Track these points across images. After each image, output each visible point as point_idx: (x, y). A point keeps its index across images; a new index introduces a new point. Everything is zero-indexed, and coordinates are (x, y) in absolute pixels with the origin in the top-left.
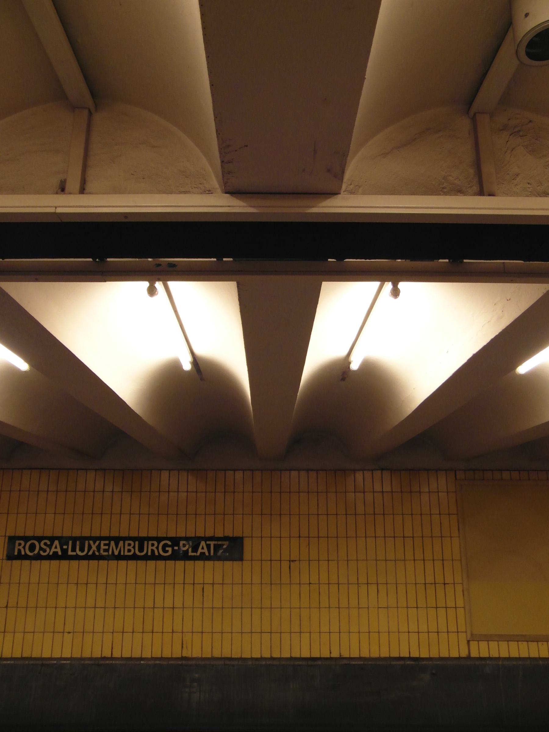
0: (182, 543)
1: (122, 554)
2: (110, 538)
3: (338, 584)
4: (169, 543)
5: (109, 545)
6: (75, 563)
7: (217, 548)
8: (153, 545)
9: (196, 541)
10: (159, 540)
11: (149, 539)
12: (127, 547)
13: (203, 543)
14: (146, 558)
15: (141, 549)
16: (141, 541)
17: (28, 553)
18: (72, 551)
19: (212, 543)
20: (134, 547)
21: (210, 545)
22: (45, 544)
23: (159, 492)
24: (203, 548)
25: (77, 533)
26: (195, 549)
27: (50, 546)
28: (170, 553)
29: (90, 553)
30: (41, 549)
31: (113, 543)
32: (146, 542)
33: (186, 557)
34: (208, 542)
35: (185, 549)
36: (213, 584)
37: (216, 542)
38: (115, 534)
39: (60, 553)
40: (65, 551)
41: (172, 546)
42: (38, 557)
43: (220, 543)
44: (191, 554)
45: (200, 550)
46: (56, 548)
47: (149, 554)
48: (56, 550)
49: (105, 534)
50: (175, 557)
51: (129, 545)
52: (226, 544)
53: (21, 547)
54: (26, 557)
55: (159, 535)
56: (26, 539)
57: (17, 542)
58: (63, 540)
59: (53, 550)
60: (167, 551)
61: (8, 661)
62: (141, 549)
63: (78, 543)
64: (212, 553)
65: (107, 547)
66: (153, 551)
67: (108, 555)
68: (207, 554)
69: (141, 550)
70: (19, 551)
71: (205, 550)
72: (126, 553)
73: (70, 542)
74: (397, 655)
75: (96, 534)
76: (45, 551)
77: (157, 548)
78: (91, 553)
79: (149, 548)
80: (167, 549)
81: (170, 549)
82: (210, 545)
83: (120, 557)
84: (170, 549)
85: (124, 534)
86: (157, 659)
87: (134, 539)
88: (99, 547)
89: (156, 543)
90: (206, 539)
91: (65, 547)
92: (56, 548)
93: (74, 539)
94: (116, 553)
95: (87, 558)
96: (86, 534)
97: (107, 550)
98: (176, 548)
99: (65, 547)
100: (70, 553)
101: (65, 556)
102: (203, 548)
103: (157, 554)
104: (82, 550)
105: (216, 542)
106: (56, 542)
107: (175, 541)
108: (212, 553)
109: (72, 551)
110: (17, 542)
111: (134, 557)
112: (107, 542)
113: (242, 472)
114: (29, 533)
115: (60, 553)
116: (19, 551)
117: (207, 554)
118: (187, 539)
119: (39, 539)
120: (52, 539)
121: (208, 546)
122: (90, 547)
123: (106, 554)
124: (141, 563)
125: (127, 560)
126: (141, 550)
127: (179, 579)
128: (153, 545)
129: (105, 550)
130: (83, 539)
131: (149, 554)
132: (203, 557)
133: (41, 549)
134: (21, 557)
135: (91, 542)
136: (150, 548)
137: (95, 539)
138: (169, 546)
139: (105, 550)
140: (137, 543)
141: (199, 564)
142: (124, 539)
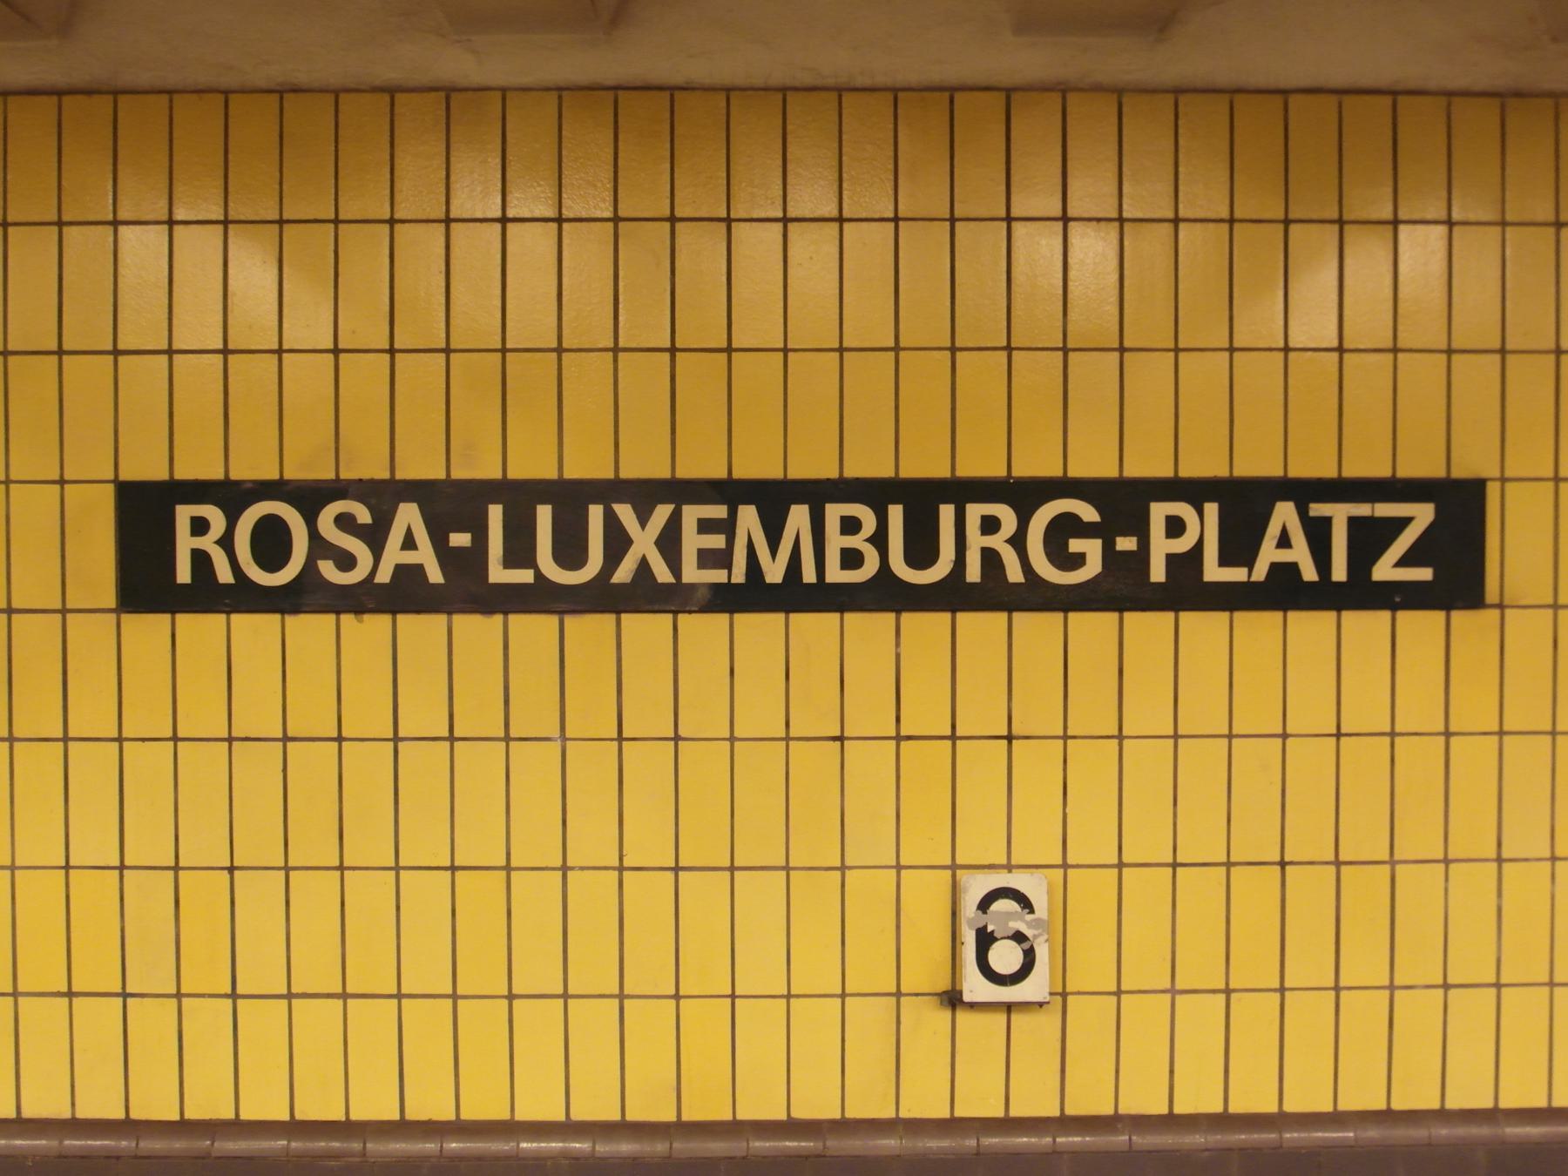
0: (1159, 512)
1: (809, 576)
2: (731, 491)
3: (732, 739)
4: (1088, 513)
5: (728, 527)
6: (534, 629)
7: (1370, 539)
8: (990, 525)
9: (1244, 505)
10: (1025, 494)
11: (963, 491)
12: (836, 541)
13: (1285, 514)
14: (953, 596)
15: (921, 550)
16: (921, 499)
18: (510, 562)
19: (1340, 514)
20: (880, 540)
21: (1327, 522)
22: (345, 522)
24: (1284, 541)
25: (532, 462)
26: (1238, 548)
27: (375, 537)
31: (748, 517)
32: (947, 513)
33: (1185, 590)
35: (1183, 545)
36: (286, 739)
37: (1363, 510)
38: (758, 464)
39: (435, 575)
41: (1103, 532)
43: (1385, 510)
44: (1214, 572)
45: (1269, 554)
46: (409, 543)
47: (973, 573)
48: (1284, 556)
49: (704, 464)
50: (1123, 589)
51: (850, 526)
52: (1422, 515)
53: (997, 542)
54: (245, 598)
55: (1022, 470)
56: (232, 496)
57: (184, 514)
58: (453, 505)
60: (1079, 560)
61: (277, 1137)
62: (921, 550)
63: (544, 514)
64: (1339, 573)
65: (717, 541)
66: (991, 558)
67: (1249, 586)
68: (1309, 573)
70: (201, 560)
71: (1300, 554)
72: (836, 574)
73: (495, 513)
74: (720, 1112)
75: (646, 461)
76: (346, 561)
77: (1018, 541)
78: (624, 573)
79: (970, 538)
80: (1075, 545)
81: (1091, 548)
82: (1327, 522)
83: (796, 596)
84: (1091, 548)
85: (813, 464)
86: (1141, 1122)
87: (877, 493)
88: (669, 542)
89: (1007, 516)
90: (1303, 491)
91: (460, 539)
92: (410, 542)
93: (520, 497)
94: (774, 572)
95: (602, 598)
96: (587, 464)
97: (721, 559)
98: (1126, 544)
99: (460, 539)
100: (498, 574)
101: (466, 591)
103: (1015, 574)
105: (1363, 510)
106: (408, 516)
107: (1123, 502)
108: (1339, 573)
109: (510, 562)
110: (184, 514)
111: (886, 595)
113: (55, 99)
114: (252, 466)
115: (435, 575)
116: (201, 560)
117: (1309, 573)
118: (1194, 491)
119: (310, 498)
120: (384, 495)
121: (1318, 534)
122: (617, 543)
124: (927, 626)
125: (841, 609)
127: (592, 712)
128: (990, 525)
129: (707, 558)
130: (570, 497)
131: (973, 573)
132: (1283, 591)
134: (205, 595)
135: (625, 512)
136: (976, 541)
137: (645, 494)
138: (1086, 530)
139: (707, 558)
140: (896, 513)
141: (1259, 626)
142: (817, 493)
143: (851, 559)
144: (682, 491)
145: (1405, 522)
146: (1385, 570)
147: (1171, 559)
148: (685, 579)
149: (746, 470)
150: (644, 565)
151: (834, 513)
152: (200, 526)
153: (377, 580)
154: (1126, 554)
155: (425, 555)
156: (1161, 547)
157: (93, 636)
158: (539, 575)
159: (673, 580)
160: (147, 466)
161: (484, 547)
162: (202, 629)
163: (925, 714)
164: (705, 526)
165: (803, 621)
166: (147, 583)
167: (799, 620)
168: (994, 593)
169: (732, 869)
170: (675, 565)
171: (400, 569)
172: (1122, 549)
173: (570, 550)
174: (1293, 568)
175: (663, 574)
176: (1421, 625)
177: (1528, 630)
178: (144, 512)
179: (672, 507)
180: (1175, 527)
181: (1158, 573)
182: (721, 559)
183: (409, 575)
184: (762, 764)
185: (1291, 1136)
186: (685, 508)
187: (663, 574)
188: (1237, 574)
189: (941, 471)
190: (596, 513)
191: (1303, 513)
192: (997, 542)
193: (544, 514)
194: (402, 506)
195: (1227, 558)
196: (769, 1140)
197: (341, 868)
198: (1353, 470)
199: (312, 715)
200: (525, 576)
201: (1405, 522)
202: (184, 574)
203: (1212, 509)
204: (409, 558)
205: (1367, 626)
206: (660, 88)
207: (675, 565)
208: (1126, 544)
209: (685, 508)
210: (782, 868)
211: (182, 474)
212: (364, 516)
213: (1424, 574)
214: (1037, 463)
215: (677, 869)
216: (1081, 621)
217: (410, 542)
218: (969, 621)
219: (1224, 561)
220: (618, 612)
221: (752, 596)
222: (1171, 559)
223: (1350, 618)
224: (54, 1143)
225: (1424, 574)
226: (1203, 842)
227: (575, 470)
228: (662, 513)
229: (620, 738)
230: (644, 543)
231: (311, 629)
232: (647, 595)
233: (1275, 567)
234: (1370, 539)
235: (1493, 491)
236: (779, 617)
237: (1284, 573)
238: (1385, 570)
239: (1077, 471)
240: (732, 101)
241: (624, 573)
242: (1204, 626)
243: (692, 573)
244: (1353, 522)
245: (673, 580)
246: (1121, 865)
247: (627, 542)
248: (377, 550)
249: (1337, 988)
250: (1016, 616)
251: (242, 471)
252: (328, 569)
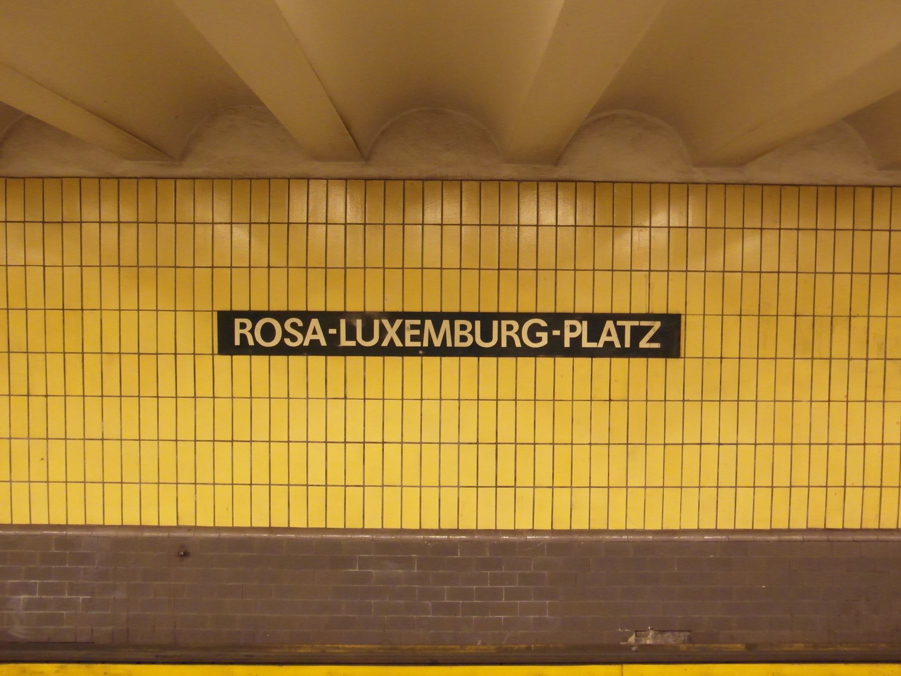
0: (568, 323)
1: (449, 344)
2: (423, 316)
4: (543, 324)
5: (421, 327)
6: (355, 361)
7: (638, 334)
9: (596, 322)
10: (522, 318)
12: (458, 333)
13: (609, 324)
14: (497, 352)
15: (486, 336)
16: (486, 319)
18: (348, 339)
19: (628, 325)
20: (473, 332)
21: (623, 327)
22: (294, 325)
24: (609, 334)
26: (594, 336)
27: (304, 331)
31: (429, 324)
32: (495, 323)
33: (575, 350)
35: (575, 335)
37: (636, 323)
38: (432, 306)
39: (323, 343)
41: (548, 330)
43: (644, 323)
44: (585, 344)
45: (604, 338)
46: (315, 332)
47: (504, 344)
48: (315, 337)
49: (413, 306)
50: (555, 349)
51: (463, 327)
52: (657, 325)
54: (258, 350)
55: (521, 310)
56: (255, 316)
57: (238, 322)
58: (329, 319)
60: (539, 340)
62: (486, 336)
64: (627, 345)
65: (417, 332)
66: (510, 340)
68: (618, 345)
70: (243, 337)
71: (614, 338)
72: (458, 344)
73: (343, 322)
75: (393, 306)
76: (294, 339)
77: (519, 333)
79: (502, 332)
80: (538, 334)
81: (544, 336)
82: (623, 327)
83: (444, 351)
84: (544, 336)
85: (451, 307)
87: (471, 317)
88: (401, 333)
90: (615, 317)
91: (332, 331)
92: (316, 332)
94: (437, 343)
95: (377, 351)
96: (374, 306)
98: (556, 333)
99: (332, 331)
100: (344, 342)
101: (332, 349)
103: (518, 344)
105: (636, 323)
106: (315, 323)
107: (556, 320)
109: (348, 339)
110: (238, 322)
111: (475, 351)
115: (323, 343)
116: (243, 337)
117: (618, 345)
118: (581, 317)
119: (281, 316)
120: (306, 316)
121: (620, 331)
122: (383, 332)
124: (488, 363)
125: (460, 356)
128: (510, 328)
129: (414, 338)
130: (368, 319)
131: (504, 344)
132: (609, 351)
134: (245, 349)
135: (386, 322)
136: (505, 333)
137: (392, 316)
138: (543, 329)
139: (414, 338)
140: (478, 324)
142: (452, 317)
143: (463, 339)
145: (650, 328)
146: (644, 344)
147: (571, 339)
149: (428, 308)
151: (458, 323)
152: (243, 326)
155: (320, 337)
156: (568, 335)
158: (357, 343)
161: (338, 335)
162: (241, 361)
163: (657, 393)
164: (413, 327)
165: (446, 360)
166: (227, 345)
168: (511, 351)
169: (232, 441)
170: (402, 340)
171: (312, 341)
172: (555, 337)
173: (368, 336)
175: (398, 343)
176: (657, 363)
177: (693, 366)
178: (226, 320)
180: (573, 329)
181: (567, 344)
182: (419, 338)
184: (450, 407)
185: (576, 537)
188: (593, 345)
189: (494, 309)
191: (615, 323)
195: (590, 340)
196: (361, 538)
198: (634, 311)
200: (352, 343)
202: (237, 342)
203: (585, 323)
205: (638, 363)
206: (850, 186)
207: (402, 340)
208: (556, 333)
212: (300, 323)
213: (656, 345)
214: (527, 307)
216: (540, 360)
217: (316, 332)
218: (502, 360)
219: (589, 340)
223: (388, 359)
224: (171, 534)
225: (656, 345)
228: (398, 322)
229: (307, 398)
230: (392, 333)
232: (392, 351)
233: (606, 343)
234: (638, 334)
238: (644, 344)
239: (540, 310)
240: (597, 188)
242: (582, 363)
243: (409, 343)
244: (632, 327)
248: (304, 336)
249: (645, 487)
252: (288, 342)
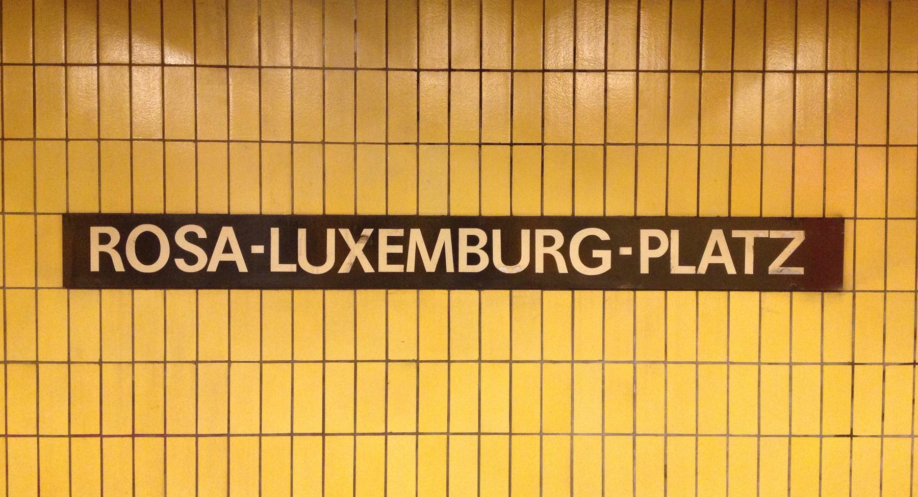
0: (645, 235)
1: (450, 268)
2: (406, 222)
4: (603, 235)
5: (404, 241)
7: (767, 250)
9: (694, 231)
10: (569, 225)
12: (464, 249)
13: (717, 236)
14: (528, 281)
15: (511, 254)
16: (511, 227)
17: (580, 267)
19: (749, 236)
20: (488, 249)
21: (742, 240)
23: (512, 71)
24: (717, 252)
26: (690, 255)
27: (208, 246)
28: (606, 266)
29: (345, 268)
30: (176, 251)
31: (416, 236)
32: (525, 234)
33: (661, 278)
34: (736, 234)
35: (659, 253)
37: (763, 234)
38: (433, 207)
39: (242, 268)
40: (259, 264)
42: (170, 279)
43: (775, 234)
44: (676, 268)
45: (707, 258)
46: (228, 249)
47: (539, 268)
48: (716, 260)
50: (624, 277)
51: (473, 240)
53: (553, 250)
54: (132, 280)
56: (125, 222)
58: (251, 228)
59: (219, 255)
60: (598, 262)
62: (511, 254)
63: (302, 234)
64: (749, 269)
65: (398, 249)
66: (549, 260)
67: (696, 276)
68: (731, 270)
69: (511, 256)
70: (105, 258)
71: (726, 260)
72: (464, 267)
73: (275, 233)
77: (565, 250)
80: (596, 254)
81: (605, 256)
82: (742, 240)
84: (605, 256)
87: (487, 223)
88: (371, 251)
90: (728, 223)
91: (258, 249)
92: (229, 249)
93: (289, 225)
94: (430, 266)
96: (309, 206)
98: (626, 251)
99: (258, 249)
100: (276, 266)
101: (259, 277)
102: (717, 252)
104: (317, 257)
105: (763, 234)
106: (227, 234)
107: (624, 229)
108: (749, 269)
110: (95, 232)
111: (489, 280)
112: (400, 233)
115: (242, 268)
116: (105, 258)
117: (731, 270)
118: (665, 223)
119: (170, 223)
120: (213, 223)
121: (737, 248)
122: (342, 250)
123: (398, 268)
126: (511, 256)
128: (549, 241)
129: (393, 259)
130: (317, 225)
131: (539, 268)
132: (717, 280)
133: (176, 251)
134: (108, 279)
135: (346, 233)
137: (356, 223)
138: (602, 245)
139: (393, 259)
140: (497, 234)
142: (455, 223)
143: (473, 259)
144: (378, 222)
145: (788, 241)
146: (775, 267)
147: (652, 261)
148: (461, 270)
150: (357, 264)
151: (464, 233)
152: (104, 239)
153: (208, 270)
154: (258, 255)
155: (237, 256)
156: (646, 254)
157: (55, 299)
158: (299, 267)
159: (372, 271)
160: (84, 204)
161: (279, 252)
167: (362, 294)
168: (550, 280)
170: (374, 262)
173: (316, 255)
174: (722, 267)
175: (367, 268)
179: (372, 230)
180: (654, 243)
181: (645, 269)
183: (227, 267)
186: (380, 230)
187: (367, 268)
188: (689, 270)
189: (442, 211)
190: (331, 233)
192: (553, 250)
193: (302, 234)
194: (714, 231)
197: (38, 436)
199: (433, 348)
200: (291, 268)
201: (789, 240)
202: (95, 266)
203: (675, 234)
204: (227, 257)
207: (374, 262)
208: (626, 251)
209: (380, 230)
210: (909, 436)
211: (330, 211)
212: (202, 234)
213: (800, 271)
215: (261, 435)
217: (229, 249)
219: (682, 262)
220: (729, 290)
221: (420, 280)
222: (652, 261)
225: (800, 271)
226: (277, 422)
227: (519, 211)
231: (181, 299)
232: (357, 280)
234: (767, 250)
235: (849, 225)
236: (756, 294)
237: (716, 270)
241: (345, 268)
244: (757, 240)
245: (372, 271)
246: (101, 436)
247: (365, 251)
250: (264, 292)
251: (173, 208)
252: (181, 263)
